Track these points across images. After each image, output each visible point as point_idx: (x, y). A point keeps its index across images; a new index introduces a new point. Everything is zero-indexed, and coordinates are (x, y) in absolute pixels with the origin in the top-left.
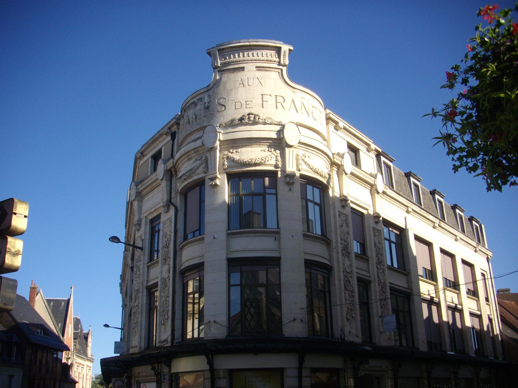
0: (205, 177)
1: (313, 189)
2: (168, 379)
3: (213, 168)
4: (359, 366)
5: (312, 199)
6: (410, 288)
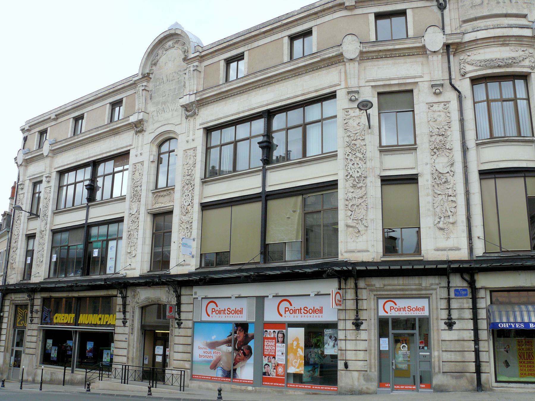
0: (531, 73)
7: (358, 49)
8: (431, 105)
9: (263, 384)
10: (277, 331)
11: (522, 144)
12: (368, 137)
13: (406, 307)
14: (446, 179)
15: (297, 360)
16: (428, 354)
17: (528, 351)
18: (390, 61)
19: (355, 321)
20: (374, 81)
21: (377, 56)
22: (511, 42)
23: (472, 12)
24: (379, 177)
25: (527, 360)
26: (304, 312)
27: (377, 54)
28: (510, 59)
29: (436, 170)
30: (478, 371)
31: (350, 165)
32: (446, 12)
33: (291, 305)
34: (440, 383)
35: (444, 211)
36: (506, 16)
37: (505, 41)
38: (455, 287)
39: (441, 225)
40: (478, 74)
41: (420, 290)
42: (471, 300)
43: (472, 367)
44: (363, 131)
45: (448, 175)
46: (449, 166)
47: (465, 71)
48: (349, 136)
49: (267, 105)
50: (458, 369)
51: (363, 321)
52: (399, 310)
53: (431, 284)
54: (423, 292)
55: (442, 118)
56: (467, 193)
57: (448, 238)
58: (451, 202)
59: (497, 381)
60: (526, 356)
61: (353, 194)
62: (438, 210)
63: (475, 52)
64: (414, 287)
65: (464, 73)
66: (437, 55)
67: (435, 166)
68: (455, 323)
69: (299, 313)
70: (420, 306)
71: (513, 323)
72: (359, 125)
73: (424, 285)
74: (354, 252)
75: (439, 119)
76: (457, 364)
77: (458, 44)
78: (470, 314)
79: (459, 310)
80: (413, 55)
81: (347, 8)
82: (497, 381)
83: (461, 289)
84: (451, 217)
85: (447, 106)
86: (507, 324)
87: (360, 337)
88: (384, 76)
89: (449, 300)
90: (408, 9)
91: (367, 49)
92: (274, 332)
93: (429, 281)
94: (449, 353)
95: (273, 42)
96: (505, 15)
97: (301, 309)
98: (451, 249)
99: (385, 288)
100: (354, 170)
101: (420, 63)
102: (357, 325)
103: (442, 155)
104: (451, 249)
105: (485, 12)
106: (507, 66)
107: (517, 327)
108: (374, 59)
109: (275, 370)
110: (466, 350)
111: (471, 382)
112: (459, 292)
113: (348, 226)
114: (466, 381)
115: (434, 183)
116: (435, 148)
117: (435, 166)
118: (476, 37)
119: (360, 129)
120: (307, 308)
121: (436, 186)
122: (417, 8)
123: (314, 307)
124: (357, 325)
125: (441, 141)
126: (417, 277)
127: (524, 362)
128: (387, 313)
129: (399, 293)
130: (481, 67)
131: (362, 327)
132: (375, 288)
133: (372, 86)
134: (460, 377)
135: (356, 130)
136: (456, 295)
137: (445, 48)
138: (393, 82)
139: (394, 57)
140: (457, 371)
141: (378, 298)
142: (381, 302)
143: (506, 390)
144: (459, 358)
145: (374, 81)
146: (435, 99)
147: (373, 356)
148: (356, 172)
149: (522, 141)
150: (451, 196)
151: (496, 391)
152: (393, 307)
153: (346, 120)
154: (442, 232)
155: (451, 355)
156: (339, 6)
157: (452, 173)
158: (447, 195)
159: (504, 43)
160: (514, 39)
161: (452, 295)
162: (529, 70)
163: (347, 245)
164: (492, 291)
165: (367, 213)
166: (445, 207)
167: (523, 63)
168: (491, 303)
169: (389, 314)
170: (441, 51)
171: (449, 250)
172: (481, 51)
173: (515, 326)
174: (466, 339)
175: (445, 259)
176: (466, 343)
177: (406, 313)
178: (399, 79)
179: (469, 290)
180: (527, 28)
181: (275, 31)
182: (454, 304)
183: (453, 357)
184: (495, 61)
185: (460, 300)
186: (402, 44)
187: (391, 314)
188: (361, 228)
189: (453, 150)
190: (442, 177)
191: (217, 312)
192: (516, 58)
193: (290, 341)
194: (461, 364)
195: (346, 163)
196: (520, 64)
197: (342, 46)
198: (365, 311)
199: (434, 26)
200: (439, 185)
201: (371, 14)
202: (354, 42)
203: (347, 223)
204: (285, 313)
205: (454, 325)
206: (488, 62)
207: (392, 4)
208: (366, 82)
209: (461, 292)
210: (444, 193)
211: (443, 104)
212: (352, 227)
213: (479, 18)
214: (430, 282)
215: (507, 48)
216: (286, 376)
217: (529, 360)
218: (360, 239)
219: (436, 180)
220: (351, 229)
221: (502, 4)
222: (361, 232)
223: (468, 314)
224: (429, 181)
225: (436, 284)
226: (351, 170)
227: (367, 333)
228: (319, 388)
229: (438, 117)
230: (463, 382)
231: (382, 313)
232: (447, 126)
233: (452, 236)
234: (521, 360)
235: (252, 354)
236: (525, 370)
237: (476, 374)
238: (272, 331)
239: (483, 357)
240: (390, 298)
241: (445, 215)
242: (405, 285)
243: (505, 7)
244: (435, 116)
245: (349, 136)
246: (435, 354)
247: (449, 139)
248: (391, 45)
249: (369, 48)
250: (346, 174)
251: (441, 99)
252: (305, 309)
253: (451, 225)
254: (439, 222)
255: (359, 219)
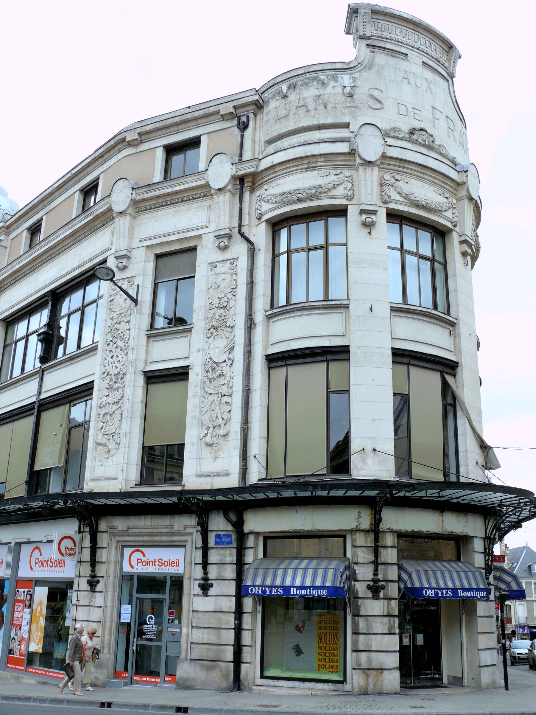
0: (347, 205)
1: (417, 232)
2: (107, 656)
3: (369, 194)
4: (494, 533)
5: (415, 250)
6: (66, 583)
7: (129, 197)
8: (214, 265)
9: (7, 667)
10: (26, 590)
11: (323, 312)
12: (134, 318)
13: (157, 560)
14: (222, 370)
15: (38, 633)
16: (178, 630)
17: (332, 631)
18: (171, 210)
19: (89, 578)
20: (149, 240)
21: (155, 204)
22: (319, 164)
23: (276, 128)
24: (142, 373)
25: (330, 644)
26: (158, 565)
27: (155, 202)
28: (314, 189)
29: (211, 359)
30: (238, 660)
31: (109, 358)
32: (248, 133)
33: (144, 556)
34: (185, 675)
35: (214, 419)
36: (320, 127)
37: (310, 163)
38: (217, 531)
39: (208, 439)
40: (274, 215)
41: (173, 534)
42: (235, 551)
43: (229, 653)
44: (129, 310)
45: (225, 364)
46: (227, 352)
47: (260, 212)
48: (112, 319)
49: (51, 284)
50: (211, 655)
51: (100, 579)
52: (148, 564)
53: (186, 526)
54: (176, 538)
55: (226, 285)
56: (247, 391)
57: (216, 458)
58: (225, 405)
59: (262, 677)
60: (328, 639)
61: (107, 398)
62: (206, 417)
63: (273, 184)
64: (164, 531)
65: (259, 215)
66: (225, 194)
67: (209, 353)
68: (211, 585)
69: (153, 566)
70: (173, 559)
71: (268, 587)
72: (125, 302)
73: (176, 527)
74: (100, 480)
75: (223, 285)
76: (211, 647)
77: (254, 176)
78: (233, 572)
79: (220, 565)
80: (199, 197)
81: (130, 144)
82: (262, 677)
83: (223, 535)
84: (222, 426)
85: (235, 264)
86: (260, 588)
87: (95, 601)
88: (155, 232)
89: (205, 550)
90: (203, 135)
91: (141, 196)
92: (24, 592)
93: (183, 522)
94: (201, 630)
95: (67, 200)
96: (319, 127)
97: (155, 561)
98: (218, 475)
99: (130, 531)
100: (113, 365)
101: (206, 208)
102: (93, 584)
103: (220, 336)
104: (218, 475)
105: (291, 126)
106: (311, 198)
107: (273, 593)
108: (153, 209)
109: (19, 647)
110: (223, 626)
111: (225, 676)
112: (221, 539)
113: (98, 444)
114: (220, 674)
115: (205, 378)
116: (213, 326)
117: (209, 353)
118: (273, 162)
119: (125, 307)
120: (162, 560)
121: (208, 383)
122: (214, 131)
123: (170, 560)
124: (93, 584)
125: (221, 316)
126: (168, 516)
127: (325, 648)
128: (133, 567)
129: (145, 538)
130: (278, 205)
131: (99, 587)
132: (117, 532)
133: (147, 247)
134: (212, 668)
135: (121, 310)
136: (216, 543)
137: (238, 182)
138: (171, 238)
139: (176, 203)
140: (209, 659)
141: (123, 547)
142: (127, 551)
143: (265, 691)
144: (213, 638)
145: (149, 239)
146: (220, 256)
147: (107, 630)
148: (114, 367)
149: (324, 308)
150: (225, 395)
151: (255, 692)
152: (141, 559)
153: (112, 296)
154: (209, 448)
155: (203, 634)
156: (122, 142)
157: (231, 362)
158: (220, 395)
159: (310, 166)
160: (322, 159)
161: (212, 542)
162: (344, 202)
163: (94, 471)
164: (268, 538)
165: (121, 423)
166: (216, 413)
167: (334, 192)
168: (265, 555)
169: (135, 570)
170: (229, 187)
171: (215, 476)
172: (281, 181)
173: (271, 591)
174: (224, 610)
175: (208, 488)
176: (224, 616)
177: (156, 569)
178: (179, 233)
179: (234, 537)
180: (341, 141)
181: (68, 185)
182: (213, 557)
183: (205, 636)
184: (293, 194)
185: (222, 551)
186: (183, 184)
187: (137, 569)
188: (112, 446)
189: (236, 328)
190: (217, 368)
191: (144, 563)
192: (322, 186)
193: (35, 606)
194: (215, 647)
195: (105, 356)
196: (330, 194)
197: (111, 196)
198: (103, 565)
199: (220, 154)
200: (212, 380)
201: (159, 148)
202: (125, 189)
203: (96, 439)
204: (137, 565)
205: (211, 589)
206: (285, 196)
207: (184, 131)
208: (140, 241)
209: (223, 539)
210: (217, 392)
211: (229, 262)
212: (101, 444)
213: (285, 136)
214: (184, 524)
215: (315, 173)
216: (26, 655)
217: (332, 645)
218: (110, 461)
219: (208, 374)
220: (100, 448)
221: (313, 111)
222: (111, 452)
223: (230, 572)
224: (200, 375)
225: (192, 526)
226: (109, 365)
227: (103, 597)
228: (44, 673)
229: (222, 282)
230: (216, 676)
231: (127, 568)
232: (231, 294)
233: (222, 454)
234: (321, 645)
235: (3, 622)
236: (325, 660)
237: (233, 664)
238: (22, 590)
239: (246, 638)
240: (138, 546)
241: (215, 425)
242: (154, 527)
243: (317, 116)
244: (219, 280)
245: (112, 319)
246: (184, 630)
247: (231, 312)
248: (170, 187)
249: (143, 194)
250: (103, 372)
251: (228, 255)
252: (160, 561)
253: (221, 439)
254: (206, 435)
255: (110, 433)
